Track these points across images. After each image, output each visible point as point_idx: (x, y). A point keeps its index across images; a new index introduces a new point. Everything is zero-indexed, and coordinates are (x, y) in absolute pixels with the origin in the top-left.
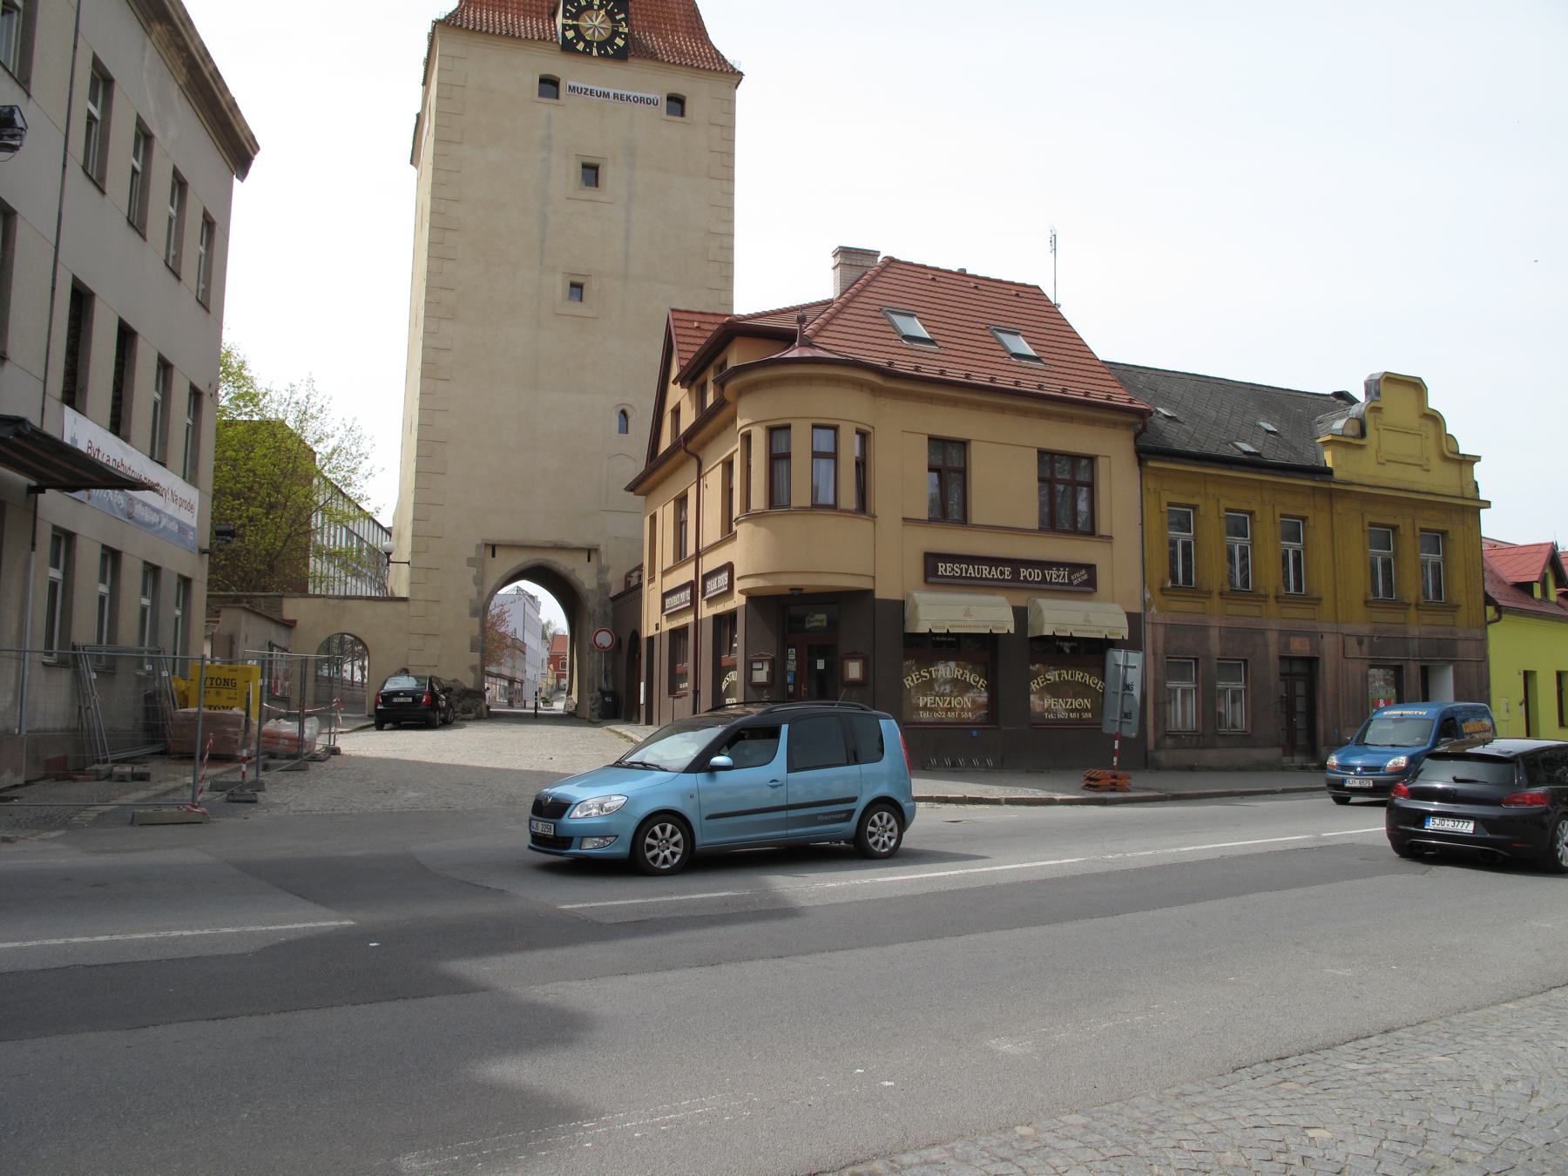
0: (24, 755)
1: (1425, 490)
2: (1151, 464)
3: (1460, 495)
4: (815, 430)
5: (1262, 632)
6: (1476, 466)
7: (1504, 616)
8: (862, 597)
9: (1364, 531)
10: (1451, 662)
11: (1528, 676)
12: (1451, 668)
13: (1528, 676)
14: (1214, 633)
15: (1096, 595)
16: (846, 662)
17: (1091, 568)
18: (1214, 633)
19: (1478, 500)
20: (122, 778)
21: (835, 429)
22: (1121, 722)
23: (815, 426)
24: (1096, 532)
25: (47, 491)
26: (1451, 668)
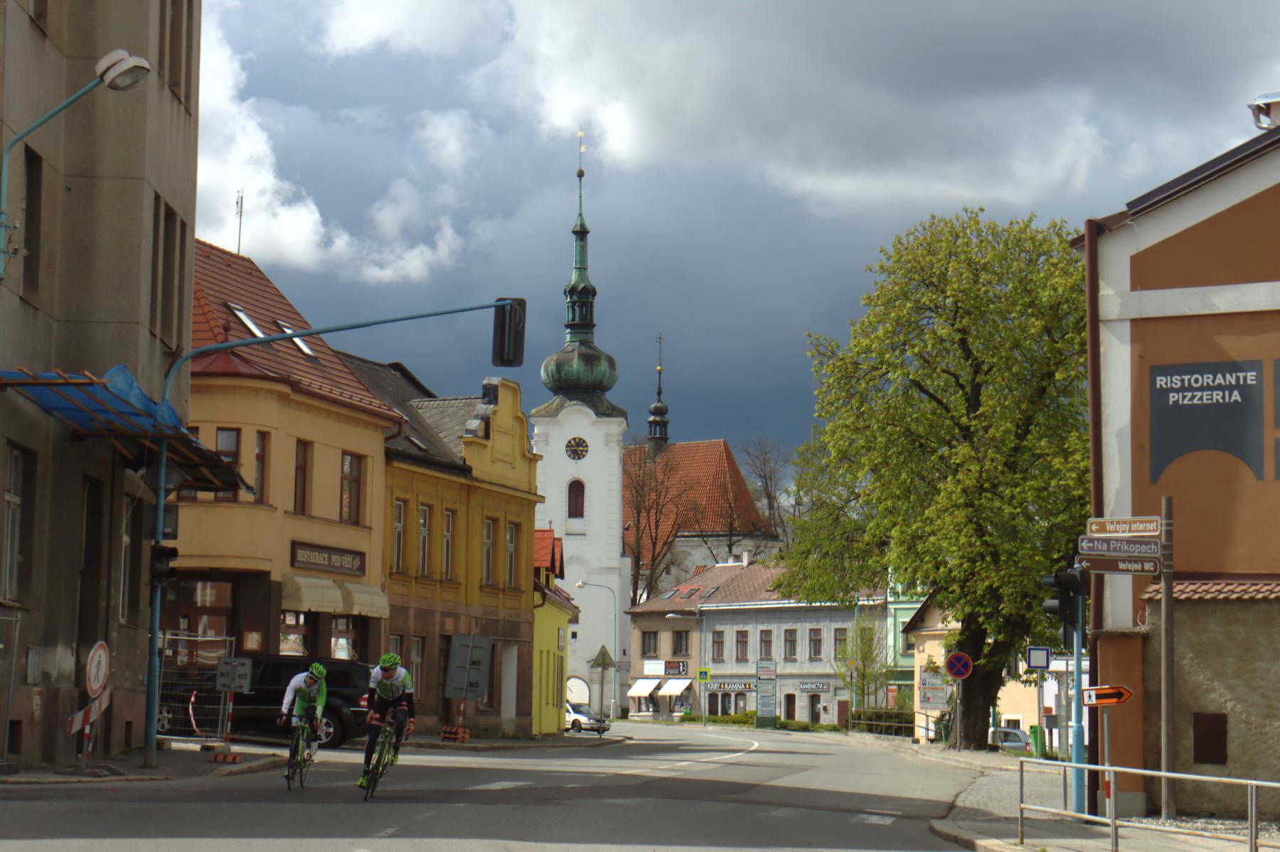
0: (904, 725)
1: (512, 486)
2: (396, 464)
3: (527, 490)
4: (219, 432)
5: (408, 608)
6: (539, 463)
7: (547, 605)
8: (265, 575)
9: (482, 523)
10: (517, 642)
11: (541, 651)
12: (516, 648)
13: (541, 651)
14: (412, 613)
15: (364, 579)
16: (246, 633)
17: (361, 555)
18: (412, 613)
19: (535, 494)
20: (548, 747)
21: (238, 431)
22: (467, 690)
23: (219, 429)
24: (361, 522)
25: (1125, 209)
26: (516, 648)
